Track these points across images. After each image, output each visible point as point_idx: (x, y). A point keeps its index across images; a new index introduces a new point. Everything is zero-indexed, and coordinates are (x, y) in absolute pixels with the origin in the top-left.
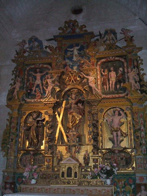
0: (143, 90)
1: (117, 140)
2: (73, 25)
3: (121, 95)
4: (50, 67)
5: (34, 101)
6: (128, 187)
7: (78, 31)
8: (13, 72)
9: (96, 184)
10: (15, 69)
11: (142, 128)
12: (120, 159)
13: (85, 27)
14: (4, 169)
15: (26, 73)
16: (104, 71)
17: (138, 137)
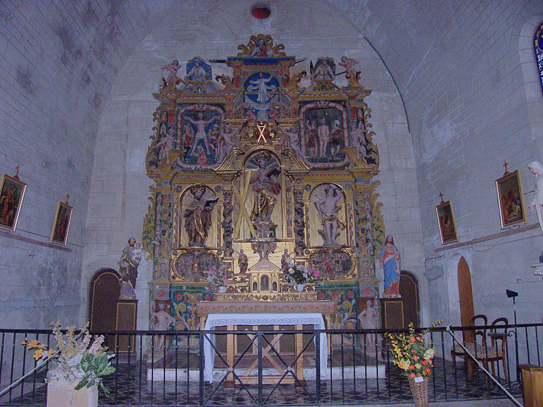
0: (371, 157)
2: (264, 44)
3: (338, 165)
4: (221, 111)
5: (196, 167)
6: (346, 303)
7: (270, 53)
8: (155, 115)
9: (306, 299)
10: (157, 109)
11: (369, 216)
12: (334, 262)
13: (283, 47)
14: (151, 279)
15: (179, 119)
16: (310, 124)
17: (363, 230)
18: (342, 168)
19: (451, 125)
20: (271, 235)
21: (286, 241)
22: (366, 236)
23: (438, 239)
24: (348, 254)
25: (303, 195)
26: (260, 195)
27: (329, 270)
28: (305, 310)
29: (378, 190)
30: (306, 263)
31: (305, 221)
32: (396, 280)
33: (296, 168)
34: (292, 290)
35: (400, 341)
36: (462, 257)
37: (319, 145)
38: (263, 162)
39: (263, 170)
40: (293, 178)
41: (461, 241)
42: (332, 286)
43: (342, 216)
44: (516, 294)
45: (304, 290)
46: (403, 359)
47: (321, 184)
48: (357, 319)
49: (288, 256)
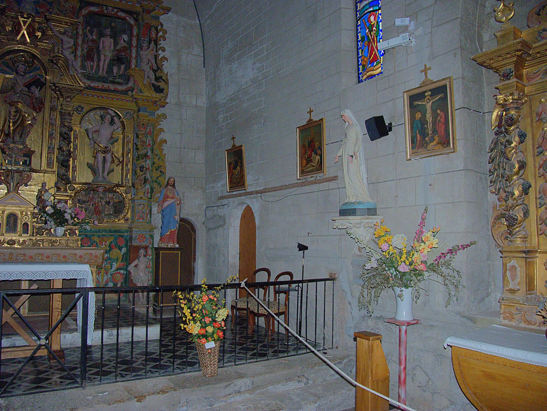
1: (104, 168)
3: (120, 88)
6: (115, 251)
9: (67, 245)
12: (104, 203)
16: (91, 32)
18: (125, 92)
19: (254, 64)
20: (25, 163)
21: (45, 172)
22: (144, 175)
23: (223, 186)
24: (121, 195)
25: (73, 118)
26: (13, 109)
27: (98, 212)
28: (65, 260)
29: (163, 125)
30: (70, 202)
31: (72, 150)
32: (174, 227)
33: (67, 82)
34: (49, 233)
35: (190, 301)
36: (248, 206)
37: (99, 60)
38: (21, 68)
39: (21, 77)
40: (62, 95)
41: (249, 190)
42: (99, 231)
43: (118, 150)
44: (306, 248)
45: (65, 235)
46: (192, 322)
47: (95, 109)
48: (126, 270)
49: (47, 191)
